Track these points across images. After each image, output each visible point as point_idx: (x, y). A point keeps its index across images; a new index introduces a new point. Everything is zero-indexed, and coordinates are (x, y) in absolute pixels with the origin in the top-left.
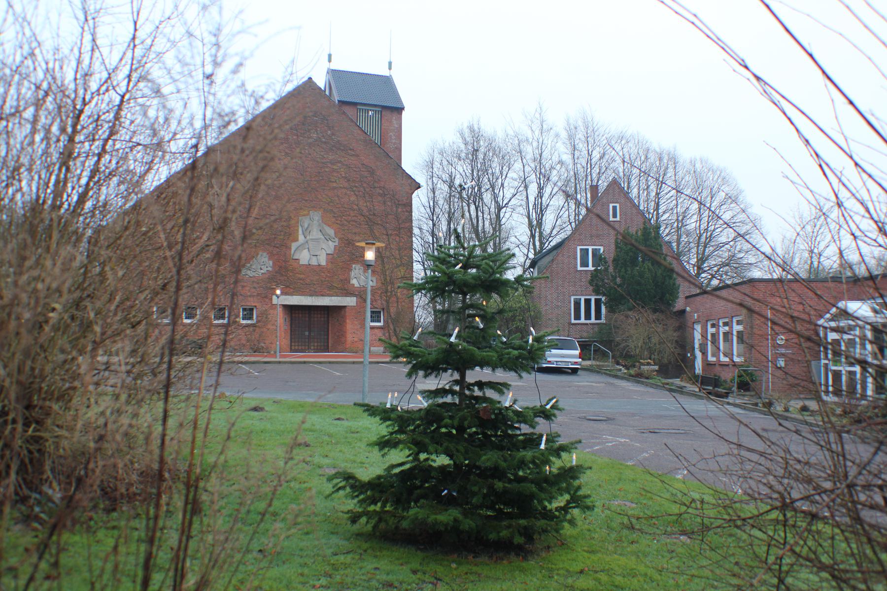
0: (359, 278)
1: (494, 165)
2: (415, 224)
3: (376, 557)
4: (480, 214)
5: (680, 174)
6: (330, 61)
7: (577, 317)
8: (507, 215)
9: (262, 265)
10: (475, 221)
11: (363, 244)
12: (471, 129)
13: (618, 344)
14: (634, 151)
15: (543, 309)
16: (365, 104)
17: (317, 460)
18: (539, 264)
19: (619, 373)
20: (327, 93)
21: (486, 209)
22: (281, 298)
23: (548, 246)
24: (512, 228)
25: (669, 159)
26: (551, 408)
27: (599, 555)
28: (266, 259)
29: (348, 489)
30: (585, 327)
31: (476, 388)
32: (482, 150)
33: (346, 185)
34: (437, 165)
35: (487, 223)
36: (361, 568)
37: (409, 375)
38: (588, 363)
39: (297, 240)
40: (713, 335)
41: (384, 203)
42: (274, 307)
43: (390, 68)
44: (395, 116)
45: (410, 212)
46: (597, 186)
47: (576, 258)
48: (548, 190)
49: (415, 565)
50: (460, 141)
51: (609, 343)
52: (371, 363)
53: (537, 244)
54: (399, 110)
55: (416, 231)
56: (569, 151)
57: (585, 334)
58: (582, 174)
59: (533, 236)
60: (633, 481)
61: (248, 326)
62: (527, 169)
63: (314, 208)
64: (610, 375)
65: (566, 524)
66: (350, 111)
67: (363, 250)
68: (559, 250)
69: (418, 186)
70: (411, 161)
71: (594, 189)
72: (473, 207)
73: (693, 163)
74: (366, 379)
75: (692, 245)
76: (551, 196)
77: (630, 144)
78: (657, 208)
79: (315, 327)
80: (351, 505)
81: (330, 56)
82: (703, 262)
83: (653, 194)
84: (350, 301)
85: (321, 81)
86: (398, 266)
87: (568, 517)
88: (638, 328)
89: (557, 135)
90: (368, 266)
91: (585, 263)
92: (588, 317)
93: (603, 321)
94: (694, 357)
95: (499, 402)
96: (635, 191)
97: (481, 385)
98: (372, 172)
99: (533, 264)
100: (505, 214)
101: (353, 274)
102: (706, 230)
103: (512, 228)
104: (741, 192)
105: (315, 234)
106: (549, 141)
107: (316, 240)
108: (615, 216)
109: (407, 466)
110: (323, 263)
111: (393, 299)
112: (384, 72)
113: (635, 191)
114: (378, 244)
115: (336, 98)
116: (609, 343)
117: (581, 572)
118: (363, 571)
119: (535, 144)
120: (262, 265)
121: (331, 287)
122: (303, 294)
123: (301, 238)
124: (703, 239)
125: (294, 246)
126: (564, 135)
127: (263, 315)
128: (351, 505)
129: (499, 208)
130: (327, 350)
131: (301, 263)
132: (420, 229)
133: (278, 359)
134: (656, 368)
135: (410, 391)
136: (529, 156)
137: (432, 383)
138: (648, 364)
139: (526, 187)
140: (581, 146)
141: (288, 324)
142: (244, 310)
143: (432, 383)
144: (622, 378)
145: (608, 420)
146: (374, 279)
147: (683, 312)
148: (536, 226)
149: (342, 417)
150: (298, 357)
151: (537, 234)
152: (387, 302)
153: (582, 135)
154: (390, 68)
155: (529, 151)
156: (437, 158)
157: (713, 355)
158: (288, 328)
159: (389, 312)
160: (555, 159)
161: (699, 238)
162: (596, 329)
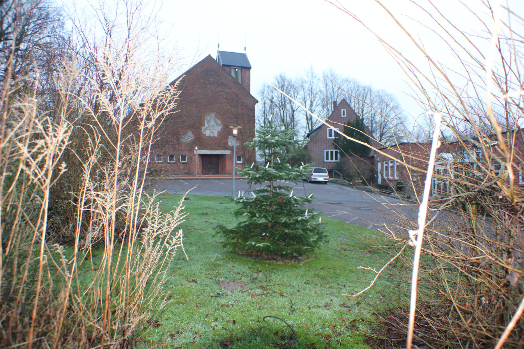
0: (232, 142)
1: (291, 92)
2: (256, 118)
3: (233, 261)
4: (285, 114)
5: (373, 96)
6: (219, 47)
7: (327, 159)
8: (297, 114)
9: (189, 137)
10: (282, 117)
11: (232, 127)
12: (281, 77)
13: (345, 171)
14: (353, 86)
15: (312, 156)
16: (234, 66)
17: (211, 221)
18: (311, 135)
19: (345, 184)
20: (218, 61)
21: (288, 112)
22: (197, 151)
23: (314, 128)
24: (299, 120)
25: (368, 90)
26: (311, 197)
27: (331, 261)
28: (191, 134)
29: (222, 233)
30: (330, 164)
31: (277, 189)
32: (286, 85)
33: (226, 101)
34: (266, 92)
35: (288, 118)
36: (226, 267)
37: (248, 183)
38: (332, 179)
39: (204, 125)
40: (386, 167)
41: (243, 109)
42: (195, 155)
43: (245, 50)
45: (254, 113)
46: (336, 102)
47: (326, 133)
48: (314, 104)
49: (250, 266)
50: (276, 82)
51: (341, 170)
52: (236, 179)
53: (310, 127)
54: (249, 68)
55: (257, 121)
56: (325, 86)
57: (331, 167)
58: (330, 96)
59: (308, 124)
60: (348, 230)
61: (183, 163)
62: (306, 94)
63: (212, 112)
64: (341, 184)
65: (317, 249)
66: (227, 69)
67: (231, 130)
68: (319, 130)
69: (257, 102)
70: (254, 92)
71: (335, 103)
72: (282, 111)
73: (378, 92)
74: (234, 186)
75: (378, 128)
76: (316, 106)
77: (351, 83)
78: (363, 112)
79: (213, 164)
80: (223, 240)
81: (219, 45)
82: (383, 135)
83: (361, 105)
84: (228, 152)
85: (215, 56)
86: (248, 137)
87: (318, 246)
88: (353, 163)
89: (319, 79)
90: (234, 136)
91: (330, 136)
92: (332, 159)
93: (338, 161)
94: (378, 177)
95: (288, 195)
96: (353, 104)
97: (280, 188)
98: (237, 96)
99: (308, 136)
100: (296, 114)
101: (229, 140)
102: (384, 121)
103: (299, 120)
104: (399, 105)
105: (213, 123)
106: (315, 81)
107: (213, 126)
108: (344, 115)
109: (247, 223)
110: (216, 136)
111: (246, 151)
112: (243, 52)
113: (353, 104)
114: (239, 127)
115: (221, 63)
116: (341, 170)
117: (322, 269)
118: (227, 268)
119: (309, 83)
120: (189, 137)
121: (220, 146)
122: (207, 149)
123: (206, 125)
124: (383, 125)
125: (203, 128)
126: (322, 79)
127: (190, 158)
128: (223, 240)
129: (293, 111)
130: (217, 173)
132: (259, 120)
133: (197, 178)
134: (361, 181)
135: (248, 191)
136: (307, 88)
137: (258, 187)
138: (358, 180)
139: (305, 102)
140: (330, 84)
141: (201, 160)
142: (182, 156)
143: (258, 187)
144: (346, 186)
145: (339, 203)
146: (238, 142)
147: (373, 157)
148: (309, 119)
149: (223, 202)
150: (205, 176)
151: (310, 123)
152: (244, 152)
153: (330, 79)
154: (245, 50)
155: (307, 86)
156: (266, 89)
157: (386, 176)
158: (200, 164)
159: (245, 157)
160: (318, 90)
161: (381, 125)
162: (335, 164)
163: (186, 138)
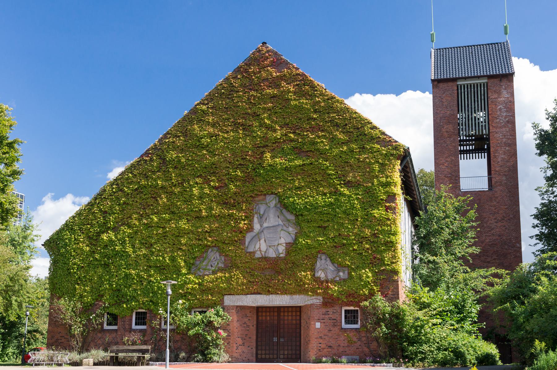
44: (504, 82)
141: (253, 330)
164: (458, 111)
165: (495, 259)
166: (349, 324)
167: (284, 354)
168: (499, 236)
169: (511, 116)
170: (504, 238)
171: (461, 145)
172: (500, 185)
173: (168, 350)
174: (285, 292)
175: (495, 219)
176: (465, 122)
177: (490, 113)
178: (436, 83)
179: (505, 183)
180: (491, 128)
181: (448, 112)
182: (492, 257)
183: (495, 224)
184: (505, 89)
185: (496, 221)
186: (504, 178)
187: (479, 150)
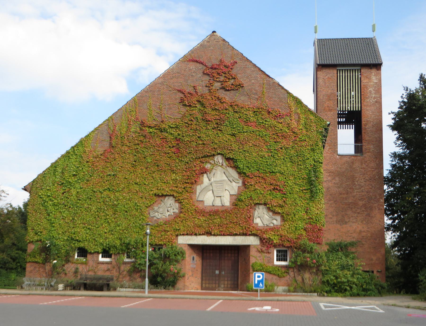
54: (378, 66)
84: (252, 241)
110: (227, 202)
125: (199, 188)
131: (206, 204)
163: (161, 210)
164: (338, 91)
165: (363, 211)
166: (279, 261)
167: (224, 284)
168: (367, 192)
169: (379, 97)
170: (371, 194)
171: (338, 118)
172: (369, 152)
173: (147, 279)
174: (231, 234)
175: (364, 179)
176: (340, 99)
177: (362, 94)
178: (320, 67)
179: (373, 151)
180: (363, 106)
181: (330, 91)
182: (361, 209)
183: (364, 183)
184: (374, 76)
185: (365, 180)
186: (372, 147)
187: (348, 122)
